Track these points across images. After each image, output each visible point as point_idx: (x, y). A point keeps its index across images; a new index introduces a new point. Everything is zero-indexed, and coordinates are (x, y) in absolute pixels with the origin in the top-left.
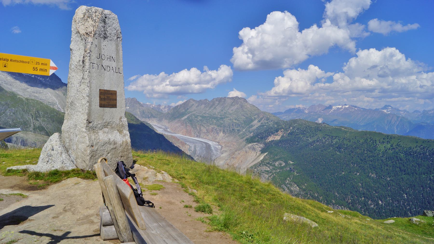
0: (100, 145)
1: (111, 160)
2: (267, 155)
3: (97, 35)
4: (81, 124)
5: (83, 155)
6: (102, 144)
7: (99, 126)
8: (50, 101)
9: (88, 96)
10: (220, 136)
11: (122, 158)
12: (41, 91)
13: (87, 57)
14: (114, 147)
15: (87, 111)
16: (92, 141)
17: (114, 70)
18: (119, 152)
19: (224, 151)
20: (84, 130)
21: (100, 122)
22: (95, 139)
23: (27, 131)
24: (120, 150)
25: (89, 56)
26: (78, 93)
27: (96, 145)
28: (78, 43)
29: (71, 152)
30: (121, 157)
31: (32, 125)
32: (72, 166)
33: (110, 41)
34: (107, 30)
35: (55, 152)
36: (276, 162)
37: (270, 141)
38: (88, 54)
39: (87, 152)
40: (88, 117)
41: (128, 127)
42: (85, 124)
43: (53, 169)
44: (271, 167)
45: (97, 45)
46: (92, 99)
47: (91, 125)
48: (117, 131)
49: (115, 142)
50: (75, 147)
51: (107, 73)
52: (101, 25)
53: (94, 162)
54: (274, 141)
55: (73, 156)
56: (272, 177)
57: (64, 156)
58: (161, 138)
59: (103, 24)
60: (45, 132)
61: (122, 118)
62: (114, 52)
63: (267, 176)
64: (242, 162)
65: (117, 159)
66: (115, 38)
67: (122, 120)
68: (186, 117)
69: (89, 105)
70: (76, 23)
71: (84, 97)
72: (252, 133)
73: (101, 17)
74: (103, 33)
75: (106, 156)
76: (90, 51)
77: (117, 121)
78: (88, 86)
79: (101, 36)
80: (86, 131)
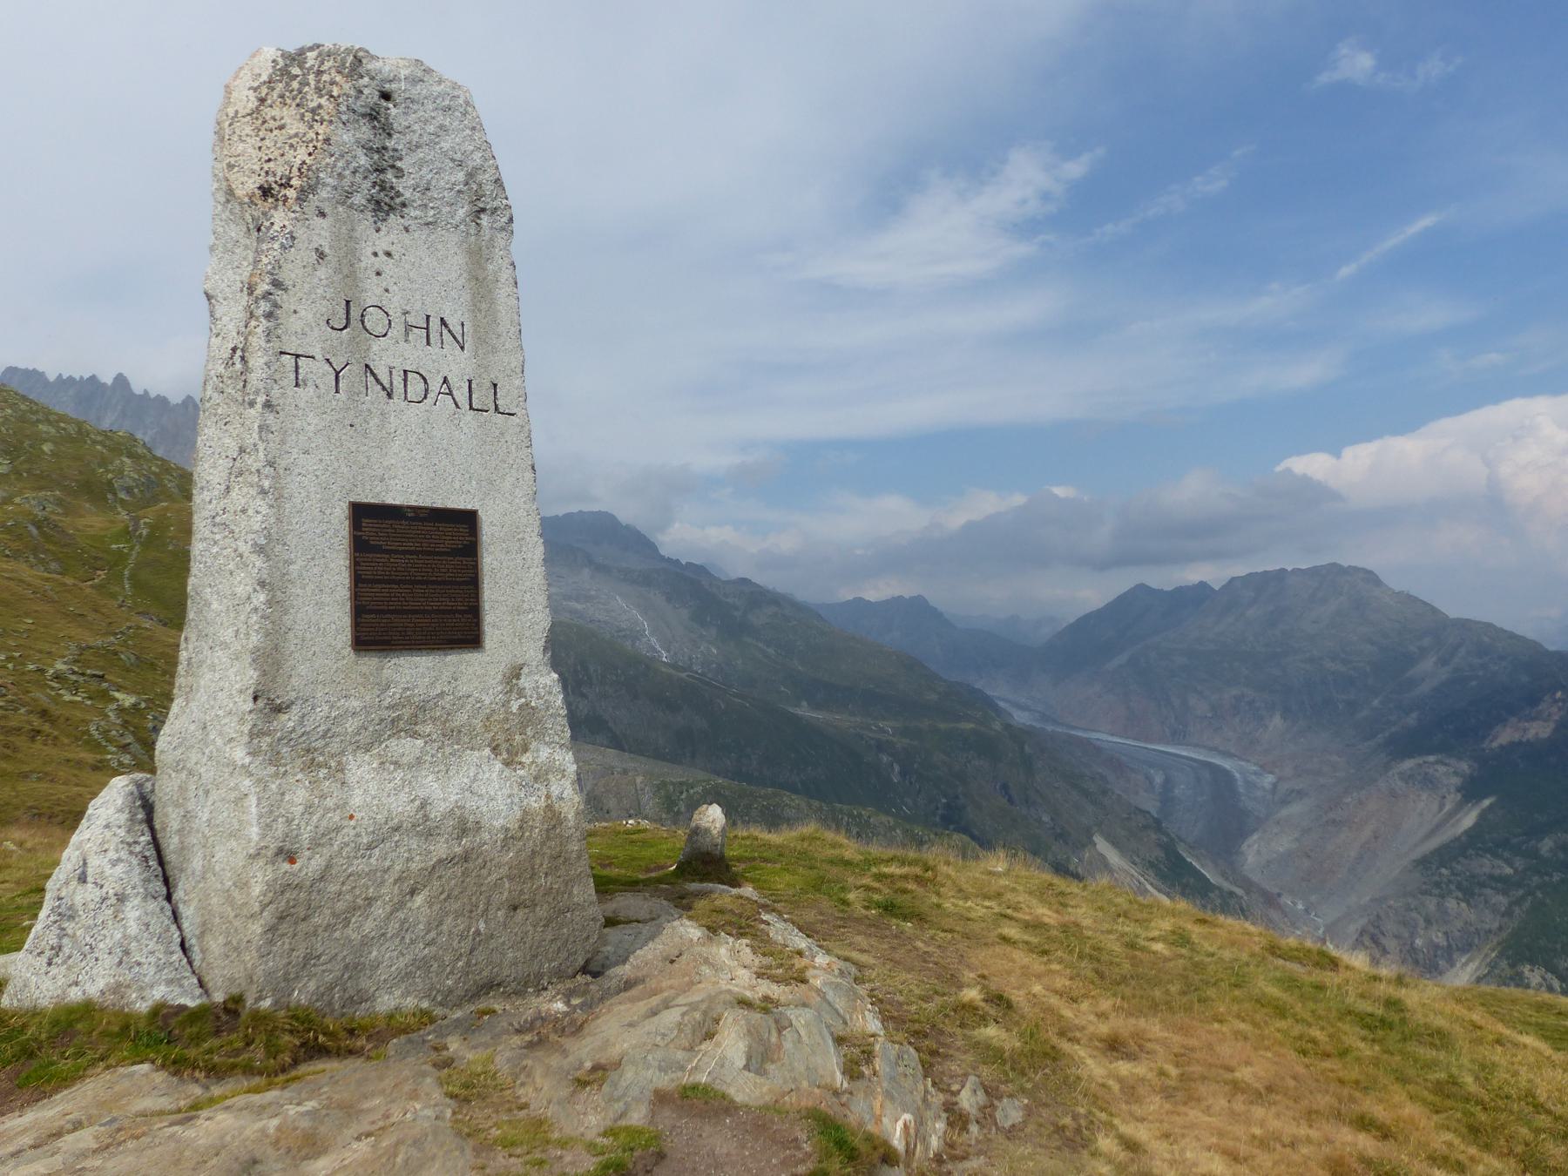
0: (347, 845)
1: (433, 934)
2: (1491, 807)
3: (324, 193)
7: (351, 725)
8: (624, 626)
9: (260, 550)
11: (520, 914)
12: (593, 593)
13: (257, 319)
14: (458, 850)
16: (289, 822)
18: (494, 876)
19: (1293, 791)
20: (240, 754)
21: (355, 704)
22: (309, 809)
25: (269, 316)
26: (218, 537)
27: (315, 844)
28: (236, 257)
30: (515, 908)
32: (169, 982)
33: (426, 231)
34: (399, 164)
36: (1542, 839)
37: (1502, 747)
38: (262, 303)
39: (249, 894)
40: (264, 673)
41: (565, 722)
42: (242, 721)
43: (75, 995)
44: (1519, 863)
45: (327, 250)
47: (288, 721)
48: (487, 751)
52: (346, 137)
53: (300, 953)
54: (1520, 743)
56: (1527, 905)
57: (133, 912)
58: (1026, 747)
59: (365, 131)
61: (525, 670)
63: (1502, 901)
64: (1376, 838)
65: (482, 926)
66: (461, 213)
67: (525, 682)
72: (1414, 715)
74: (367, 184)
77: (485, 690)
78: (263, 492)
79: (358, 199)
80: (247, 760)
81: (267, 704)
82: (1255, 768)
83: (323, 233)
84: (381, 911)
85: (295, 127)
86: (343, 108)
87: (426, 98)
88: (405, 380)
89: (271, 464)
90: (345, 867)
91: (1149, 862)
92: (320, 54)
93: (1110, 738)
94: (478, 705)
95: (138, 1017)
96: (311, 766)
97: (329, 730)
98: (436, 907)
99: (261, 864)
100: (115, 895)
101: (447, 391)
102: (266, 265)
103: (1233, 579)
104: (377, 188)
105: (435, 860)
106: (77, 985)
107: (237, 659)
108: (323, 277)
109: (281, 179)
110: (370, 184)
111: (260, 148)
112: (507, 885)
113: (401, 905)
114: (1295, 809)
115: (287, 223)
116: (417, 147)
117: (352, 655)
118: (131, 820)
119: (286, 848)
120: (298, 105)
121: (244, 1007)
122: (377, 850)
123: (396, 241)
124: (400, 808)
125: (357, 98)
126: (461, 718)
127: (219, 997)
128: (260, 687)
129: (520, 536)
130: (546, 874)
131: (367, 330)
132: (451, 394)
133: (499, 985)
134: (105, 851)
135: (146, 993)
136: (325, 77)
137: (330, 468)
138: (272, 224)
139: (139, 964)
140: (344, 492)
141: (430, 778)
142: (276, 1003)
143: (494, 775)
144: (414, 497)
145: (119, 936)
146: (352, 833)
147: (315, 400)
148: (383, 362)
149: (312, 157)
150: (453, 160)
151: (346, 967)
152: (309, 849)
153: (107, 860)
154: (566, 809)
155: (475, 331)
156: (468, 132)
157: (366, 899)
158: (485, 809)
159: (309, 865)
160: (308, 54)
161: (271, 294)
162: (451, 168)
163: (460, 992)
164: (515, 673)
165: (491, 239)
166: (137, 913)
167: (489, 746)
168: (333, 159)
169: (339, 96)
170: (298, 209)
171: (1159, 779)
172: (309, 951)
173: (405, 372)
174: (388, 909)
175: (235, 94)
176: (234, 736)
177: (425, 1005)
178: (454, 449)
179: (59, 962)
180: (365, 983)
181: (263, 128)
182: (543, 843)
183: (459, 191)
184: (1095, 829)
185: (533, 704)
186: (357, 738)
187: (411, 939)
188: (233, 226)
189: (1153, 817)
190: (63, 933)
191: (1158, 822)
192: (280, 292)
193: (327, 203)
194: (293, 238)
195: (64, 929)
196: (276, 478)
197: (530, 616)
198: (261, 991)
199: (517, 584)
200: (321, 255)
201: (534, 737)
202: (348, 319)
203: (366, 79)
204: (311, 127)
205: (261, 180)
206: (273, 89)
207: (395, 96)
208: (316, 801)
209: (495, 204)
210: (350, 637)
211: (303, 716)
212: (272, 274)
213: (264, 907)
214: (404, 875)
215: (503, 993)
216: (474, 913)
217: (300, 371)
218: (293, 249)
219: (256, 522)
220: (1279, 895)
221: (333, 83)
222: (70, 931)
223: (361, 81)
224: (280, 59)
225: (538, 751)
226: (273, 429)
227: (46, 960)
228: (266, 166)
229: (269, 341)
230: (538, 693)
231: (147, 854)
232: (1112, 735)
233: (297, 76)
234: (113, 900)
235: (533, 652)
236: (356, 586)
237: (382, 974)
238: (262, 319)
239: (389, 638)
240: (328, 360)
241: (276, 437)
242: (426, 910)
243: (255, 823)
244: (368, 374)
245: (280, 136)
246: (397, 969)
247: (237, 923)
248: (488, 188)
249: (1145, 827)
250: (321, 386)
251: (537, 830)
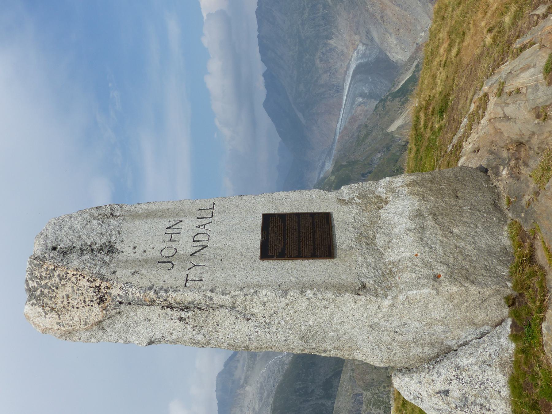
4: (369, 311)
5: (466, 304)
6: (427, 249)
7: (370, 260)
8: (277, 369)
9: (285, 293)
10: (336, 45)
11: (459, 195)
13: (168, 297)
14: (430, 217)
15: (330, 295)
16: (420, 278)
17: (205, 221)
18: (442, 204)
20: (386, 303)
21: (360, 258)
23: (333, 410)
24: (437, 202)
25: (166, 291)
26: (276, 322)
27: (430, 267)
28: (132, 325)
29: (453, 339)
30: (457, 197)
31: (320, 402)
32: (499, 338)
34: (89, 244)
35: (454, 387)
38: (160, 294)
40: (347, 291)
42: (370, 302)
43: (505, 392)
45: (133, 270)
46: (293, 280)
47: (369, 283)
48: (381, 211)
49: (416, 216)
50: (439, 329)
51: (215, 241)
52: (75, 263)
53: (484, 272)
55: (464, 335)
57: (464, 362)
58: (343, 164)
59: (73, 256)
60: (333, 378)
61: (340, 198)
62: (154, 224)
65: (466, 208)
66: (113, 222)
67: (347, 198)
68: (300, 115)
69: (311, 288)
70: (74, 332)
71: (287, 305)
73: (53, 260)
74: (99, 255)
75: (461, 238)
76: (150, 288)
78: (256, 292)
80: (390, 297)
81: (362, 290)
82: (355, 53)
83: (124, 272)
84: (462, 244)
85: (68, 289)
86: (61, 264)
87: (55, 234)
88: (198, 241)
89: (242, 289)
90: (441, 257)
91: (401, 106)
92: (31, 279)
93: (340, 122)
94: (359, 214)
95: (517, 346)
96: (392, 274)
97: (373, 268)
98: (459, 224)
99: (441, 288)
100: (455, 371)
101: (203, 226)
102: (140, 293)
103: (262, 60)
104: (101, 251)
105: (435, 225)
106: (500, 392)
107: (339, 307)
108: (147, 271)
109: (95, 292)
110: (99, 254)
111: (77, 308)
112: (446, 199)
113: (459, 237)
114: (375, 35)
115: (119, 287)
116: (80, 237)
117: (336, 259)
118: (417, 372)
119: (433, 278)
120: (57, 288)
121: (511, 294)
122: (432, 246)
123: (128, 245)
124: (411, 238)
125: (55, 259)
126: (365, 221)
127: (506, 311)
128: (354, 292)
129: (275, 200)
130: (440, 185)
131: (173, 255)
132: (204, 225)
133: (494, 202)
134: (433, 381)
135: (505, 347)
136: (44, 274)
137: (243, 268)
138: (118, 295)
139: (490, 355)
140: (255, 262)
141: (395, 230)
142: (509, 280)
143: (392, 207)
144: (257, 237)
145: (476, 367)
146: (424, 254)
147: (209, 273)
148: (189, 249)
149: (85, 276)
150: (87, 224)
151: (490, 255)
152: (433, 270)
153: (437, 379)
154: (408, 180)
155: (173, 217)
156: (72, 219)
157: (456, 248)
158: (410, 208)
159: (440, 269)
160: (30, 286)
161: (155, 291)
162: (91, 225)
163: (499, 215)
164: (342, 201)
165: (126, 211)
166: (465, 359)
167: (378, 210)
168: (86, 267)
169: (55, 266)
170: (112, 281)
171: (360, 100)
172: (483, 269)
173: (193, 241)
174: (460, 241)
175: (48, 326)
176: (377, 306)
177: (506, 228)
178: (232, 223)
179: (488, 405)
180: (497, 249)
181: (67, 308)
182: (425, 187)
183: (103, 222)
184: (384, 131)
185: (357, 195)
186: (377, 258)
187: (475, 233)
188: (115, 326)
189: (379, 103)
190: (474, 403)
191: (381, 101)
192: (155, 287)
193: (109, 270)
194: (127, 283)
195: (472, 403)
196: (249, 287)
197: (314, 196)
198: (504, 287)
199: (298, 201)
200: (135, 272)
201: (373, 194)
202: (168, 262)
203: (46, 255)
204: (70, 279)
205: (95, 304)
206: (47, 304)
207: (54, 245)
208: (409, 269)
209: (109, 209)
210: (327, 260)
211: (366, 277)
212: (145, 290)
213: (462, 285)
214: (444, 235)
215: (498, 201)
216: (461, 211)
217: (194, 279)
218: (133, 283)
219: (271, 295)
220: (417, 44)
221: (47, 270)
222: (473, 399)
223: (47, 257)
224: (32, 302)
225: (380, 192)
226: (224, 288)
227: (487, 412)
228: (88, 303)
229: (180, 291)
230: (352, 193)
231: (434, 362)
232: (338, 121)
233: (41, 291)
234: (458, 372)
235: (332, 195)
236: (302, 257)
237: (493, 243)
238: (168, 294)
239: (327, 245)
240: (188, 269)
241: (228, 288)
242: (460, 227)
243: (421, 291)
244: (195, 254)
245: (73, 296)
246: (489, 237)
247: (470, 301)
248: (100, 212)
249: (384, 107)
250: (202, 271)
251: (419, 189)
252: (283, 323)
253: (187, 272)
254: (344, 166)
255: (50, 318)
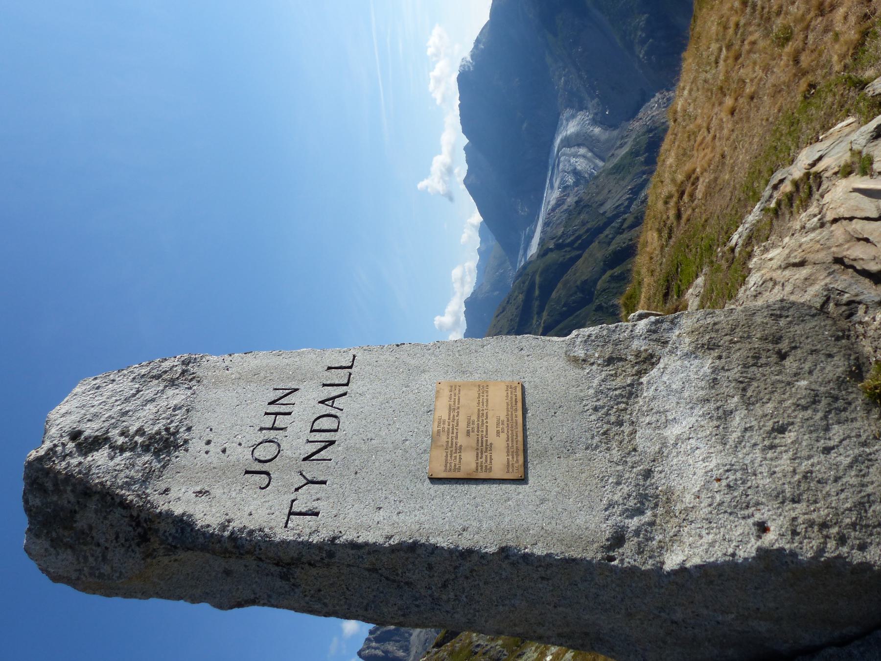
173: (312, 431)
252: (465, 599)
253: (293, 497)
254: (551, 250)
255: (62, 561)
